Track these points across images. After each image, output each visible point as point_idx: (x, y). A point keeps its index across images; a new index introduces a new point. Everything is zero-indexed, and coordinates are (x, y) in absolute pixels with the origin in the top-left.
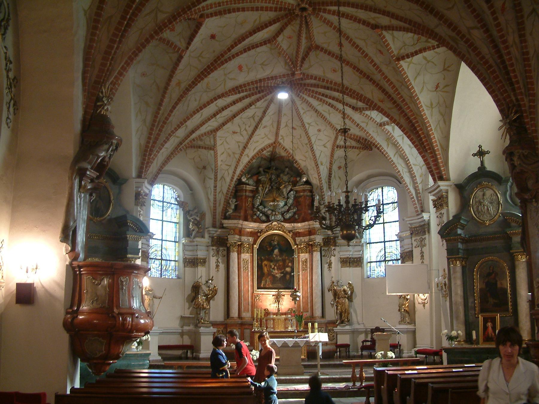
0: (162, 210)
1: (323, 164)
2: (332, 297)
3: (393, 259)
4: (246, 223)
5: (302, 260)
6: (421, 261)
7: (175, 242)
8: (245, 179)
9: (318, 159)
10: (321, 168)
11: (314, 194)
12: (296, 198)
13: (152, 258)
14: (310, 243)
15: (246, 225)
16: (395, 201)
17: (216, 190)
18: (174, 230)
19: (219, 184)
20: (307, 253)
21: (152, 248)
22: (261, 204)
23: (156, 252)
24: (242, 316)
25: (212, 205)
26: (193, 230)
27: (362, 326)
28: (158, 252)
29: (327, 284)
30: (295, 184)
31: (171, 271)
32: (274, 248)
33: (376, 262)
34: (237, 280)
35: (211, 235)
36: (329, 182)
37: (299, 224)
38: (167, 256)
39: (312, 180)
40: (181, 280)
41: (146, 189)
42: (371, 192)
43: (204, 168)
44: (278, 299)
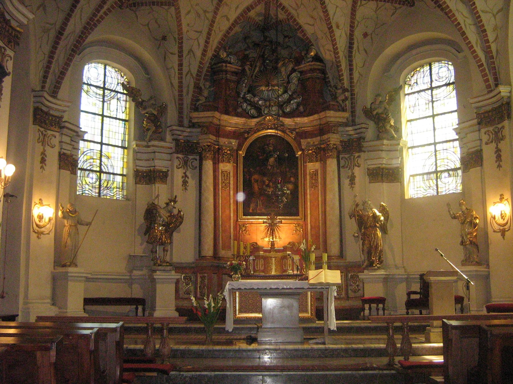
0: (102, 100)
1: (340, 28)
2: (355, 227)
3: (449, 168)
4: (225, 117)
5: (310, 172)
6: (497, 164)
7: (123, 147)
8: (225, 55)
9: (331, 17)
10: (338, 33)
11: (327, 76)
12: (302, 82)
13: (85, 168)
14: (322, 146)
15: (225, 120)
16: (451, 82)
17: (181, 70)
18: (122, 130)
19: (185, 63)
20: (317, 161)
21: (85, 154)
22: (249, 92)
23: (92, 161)
24: (220, 255)
25: (177, 93)
26: (148, 130)
27: (401, 271)
28: (95, 160)
29: (348, 205)
30: (298, 61)
31: (115, 190)
32: (269, 155)
33: (423, 174)
34: (211, 200)
35: (175, 137)
36: (350, 56)
37: (306, 119)
38: (109, 167)
39: (324, 56)
40: (130, 202)
41: (11, 4)
42: (413, 73)
43: (164, 38)
44: (272, 229)
